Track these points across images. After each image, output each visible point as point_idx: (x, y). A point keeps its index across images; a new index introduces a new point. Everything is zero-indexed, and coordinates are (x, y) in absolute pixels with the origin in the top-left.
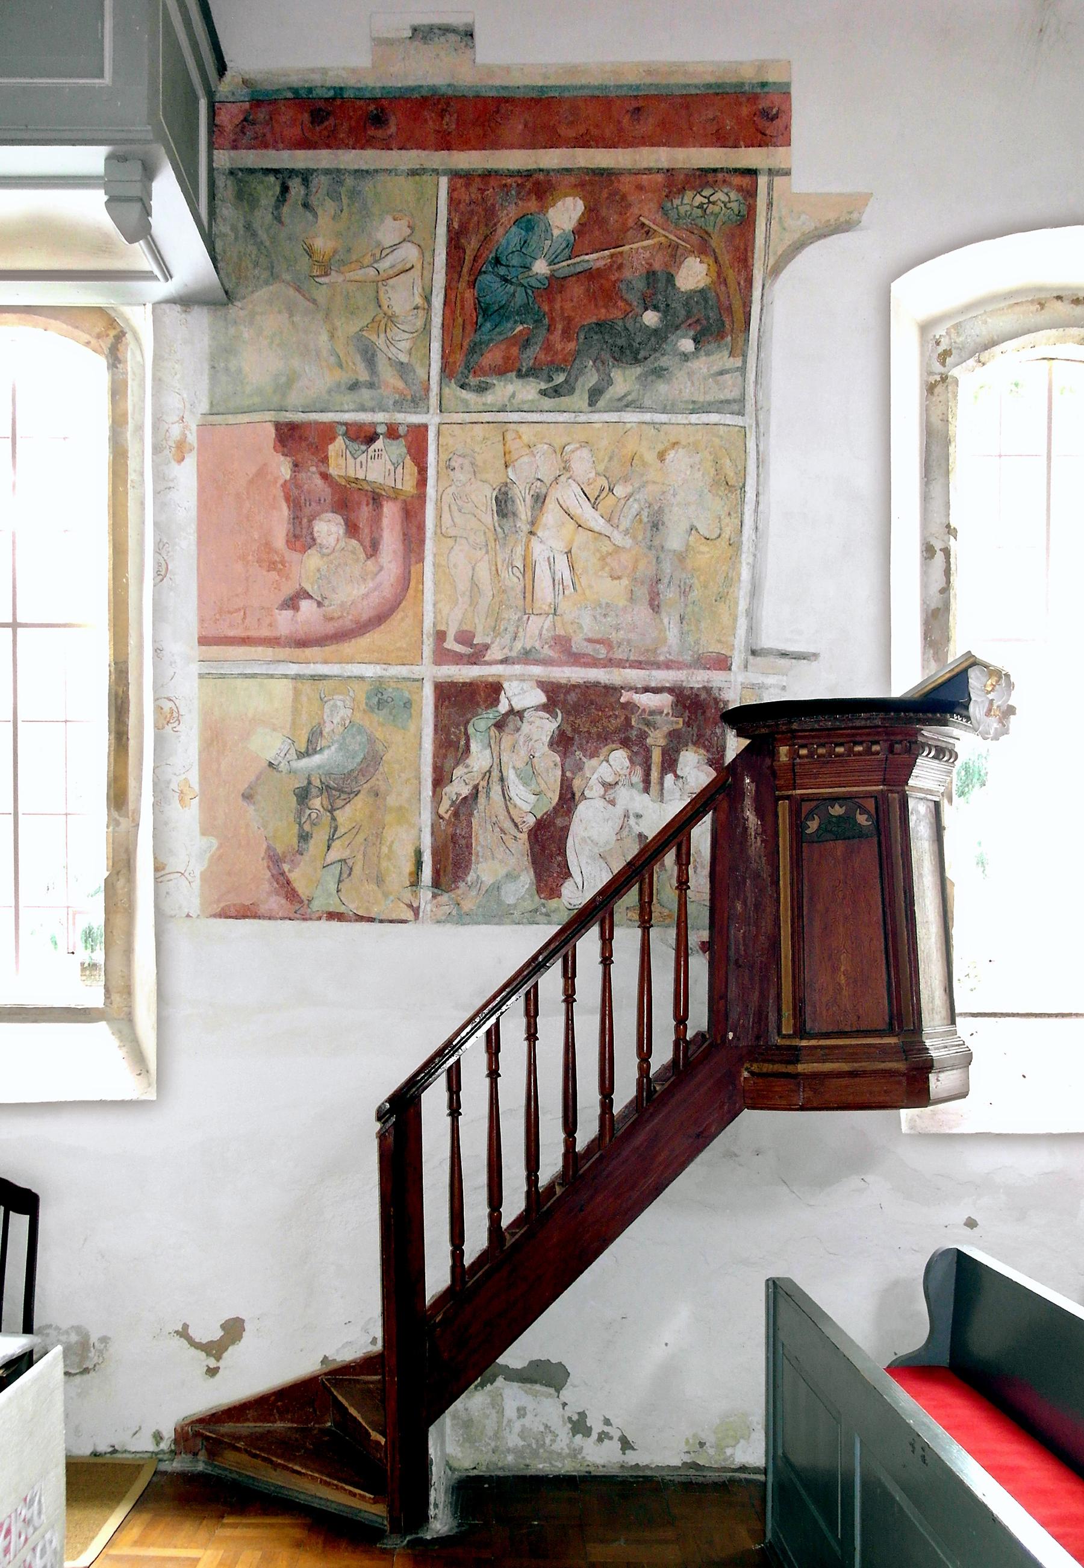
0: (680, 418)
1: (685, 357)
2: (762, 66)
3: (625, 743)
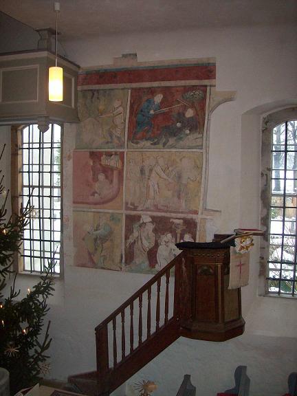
0: (186, 150)
1: (187, 135)
2: (209, 59)
3: (171, 232)
